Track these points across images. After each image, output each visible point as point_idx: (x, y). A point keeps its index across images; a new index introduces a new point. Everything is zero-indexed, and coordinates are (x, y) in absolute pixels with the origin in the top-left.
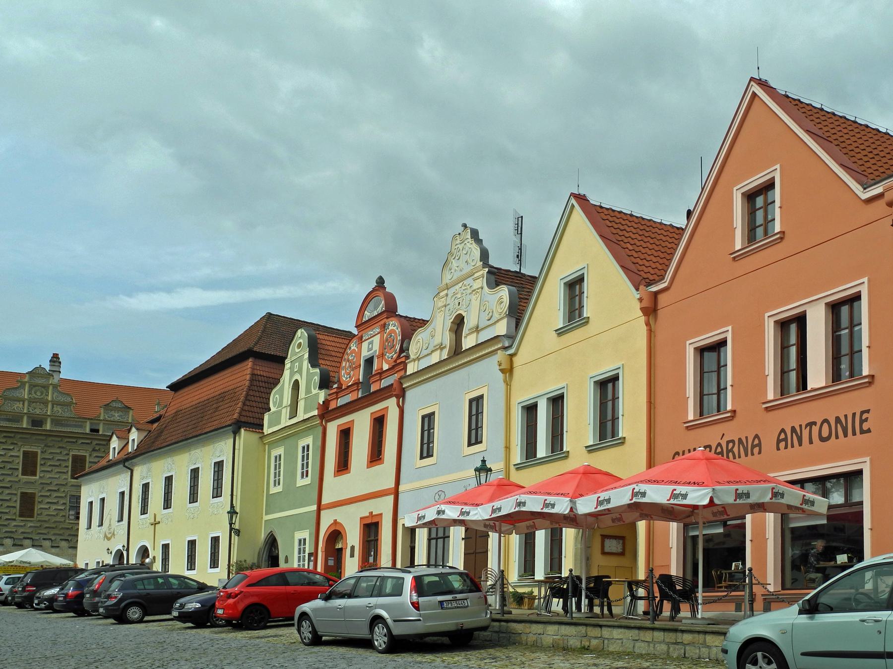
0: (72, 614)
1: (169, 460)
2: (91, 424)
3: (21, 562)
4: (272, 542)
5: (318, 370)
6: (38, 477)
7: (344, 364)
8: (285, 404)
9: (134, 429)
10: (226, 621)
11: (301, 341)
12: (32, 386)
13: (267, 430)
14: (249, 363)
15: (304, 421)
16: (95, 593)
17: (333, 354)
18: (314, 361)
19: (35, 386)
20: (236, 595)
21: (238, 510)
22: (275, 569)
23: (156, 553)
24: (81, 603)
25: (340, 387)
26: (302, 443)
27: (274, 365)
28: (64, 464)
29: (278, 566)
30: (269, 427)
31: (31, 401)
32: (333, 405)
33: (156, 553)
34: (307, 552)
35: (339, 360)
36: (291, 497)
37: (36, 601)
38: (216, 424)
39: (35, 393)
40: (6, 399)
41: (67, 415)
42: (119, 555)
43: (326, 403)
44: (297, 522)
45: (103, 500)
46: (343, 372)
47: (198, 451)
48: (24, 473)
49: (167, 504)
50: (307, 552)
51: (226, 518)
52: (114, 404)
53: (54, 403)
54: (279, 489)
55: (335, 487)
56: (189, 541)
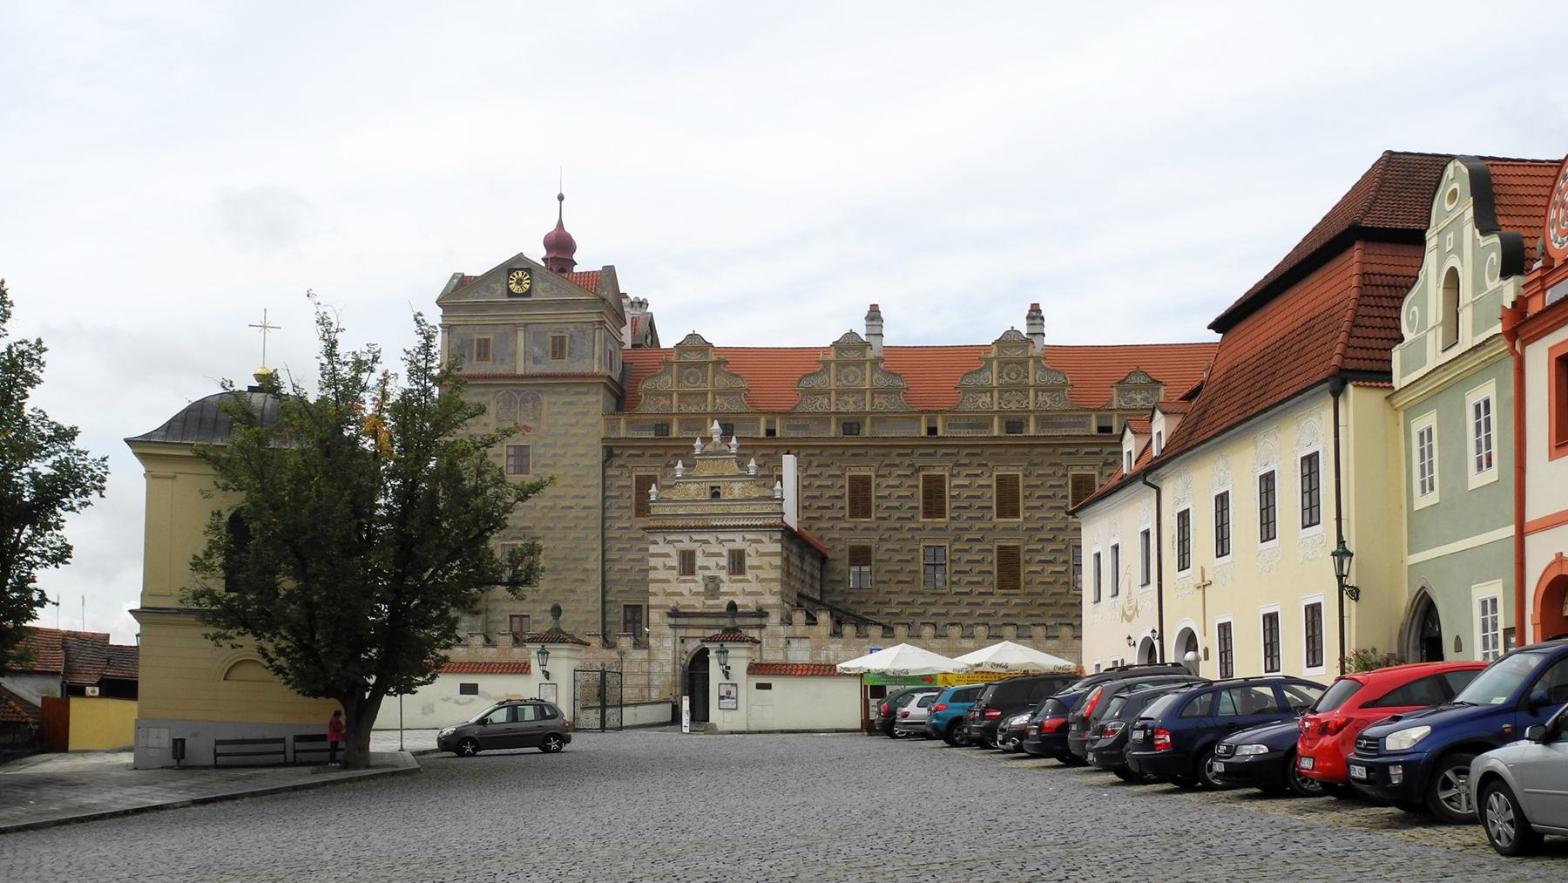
0: (1055, 761)
1: (1221, 463)
2: (1098, 418)
3: (994, 665)
4: (1425, 613)
5: (1495, 239)
6: (947, 519)
7: (1553, 214)
8: (1431, 322)
9: (1158, 414)
10: (1322, 784)
11: (1456, 185)
12: (1004, 363)
13: (1398, 381)
14: (1356, 254)
15: (1475, 349)
16: (1085, 722)
17: (1529, 201)
18: (1485, 222)
19: (1007, 363)
20: (1339, 728)
21: (1351, 546)
22: (1438, 665)
23: (1209, 640)
24: (1064, 741)
25: (1548, 267)
26: (1474, 396)
27: (1410, 250)
28: (1060, 493)
29: (1441, 658)
30: (1402, 376)
31: (1003, 390)
32: (1535, 307)
33: (1209, 640)
34: (1501, 626)
35: (1543, 211)
36: (1459, 512)
37: (1000, 737)
38: (1300, 382)
39: (846, 378)
40: (966, 390)
41: (1057, 406)
42: (1149, 649)
43: (1520, 304)
44: (1475, 565)
45: (1116, 548)
46: (1553, 232)
47: (1271, 440)
48: (927, 514)
49: (1222, 547)
50: (1501, 626)
51: (1330, 566)
52: (1133, 379)
53: (1039, 389)
54: (1433, 498)
56: (1220, 626)
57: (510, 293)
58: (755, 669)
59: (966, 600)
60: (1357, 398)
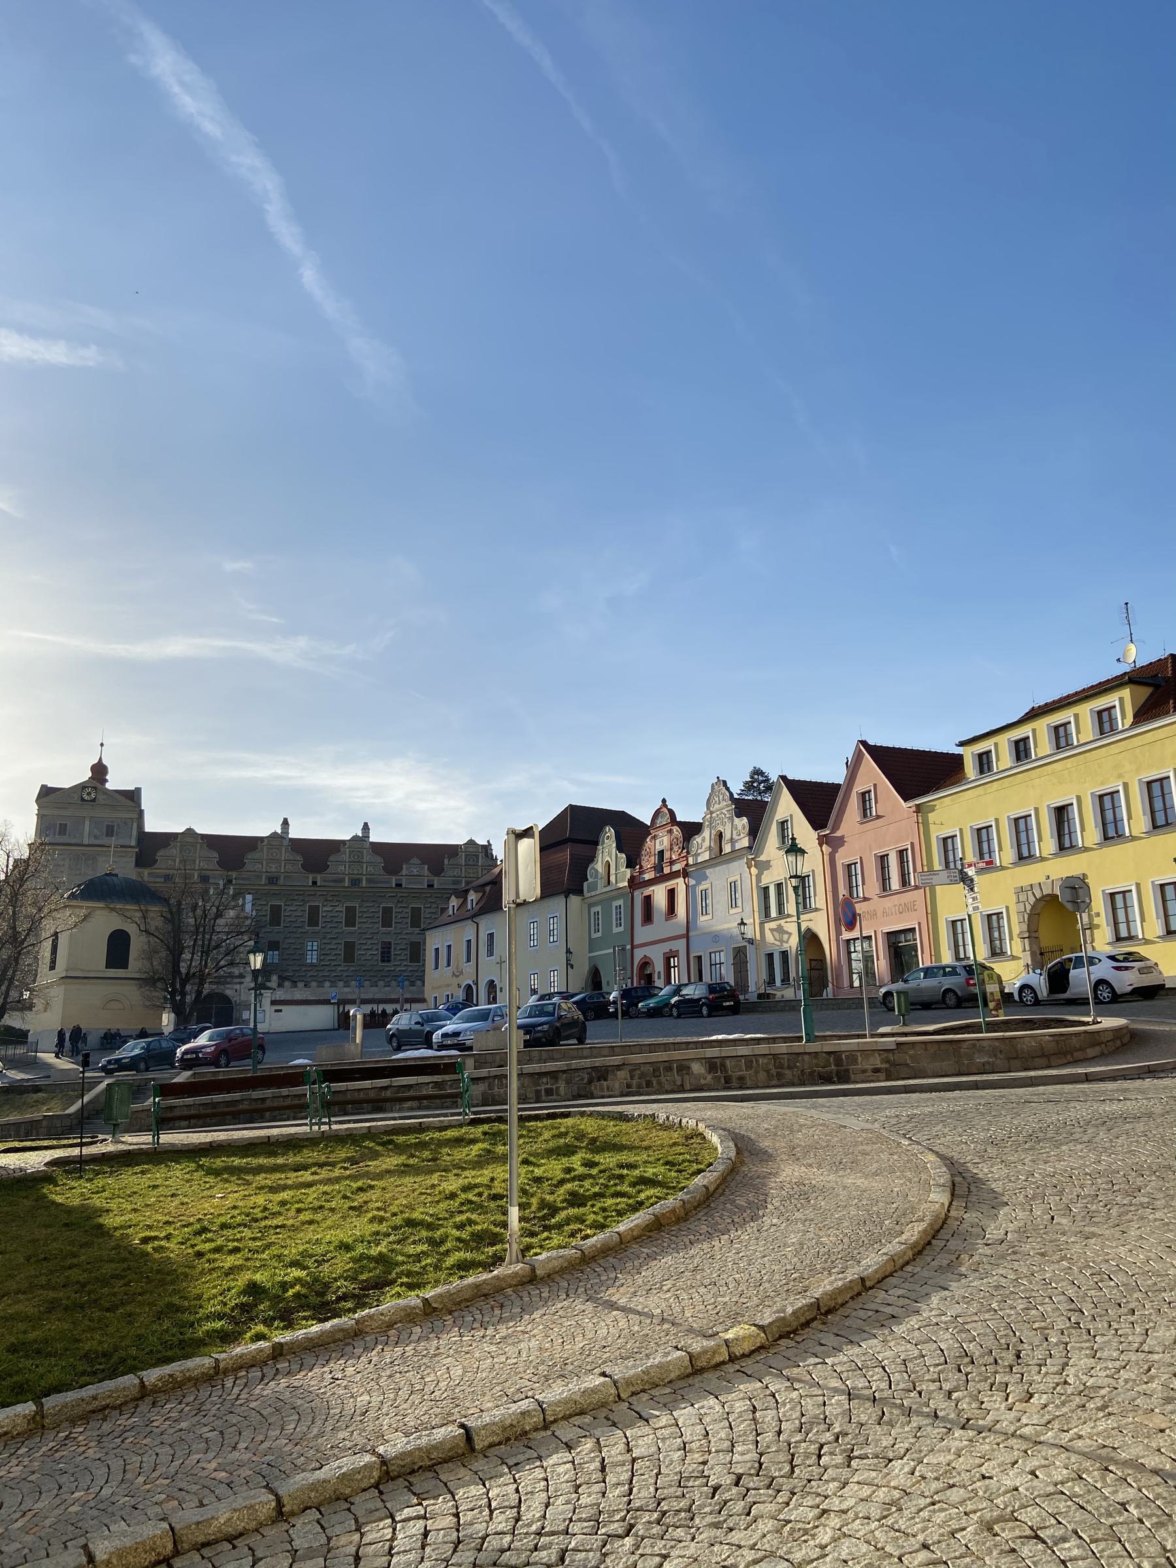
18: (620, 848)
45: (449, 946)
54: (599, 934)
55: (643, 933)
57: (83, 799)
58: (273, 1003)
59: (327, 968)
60: (574, 900)
